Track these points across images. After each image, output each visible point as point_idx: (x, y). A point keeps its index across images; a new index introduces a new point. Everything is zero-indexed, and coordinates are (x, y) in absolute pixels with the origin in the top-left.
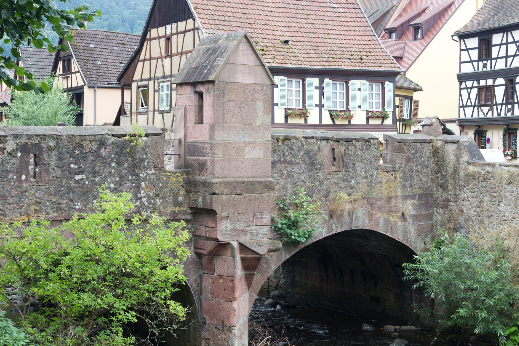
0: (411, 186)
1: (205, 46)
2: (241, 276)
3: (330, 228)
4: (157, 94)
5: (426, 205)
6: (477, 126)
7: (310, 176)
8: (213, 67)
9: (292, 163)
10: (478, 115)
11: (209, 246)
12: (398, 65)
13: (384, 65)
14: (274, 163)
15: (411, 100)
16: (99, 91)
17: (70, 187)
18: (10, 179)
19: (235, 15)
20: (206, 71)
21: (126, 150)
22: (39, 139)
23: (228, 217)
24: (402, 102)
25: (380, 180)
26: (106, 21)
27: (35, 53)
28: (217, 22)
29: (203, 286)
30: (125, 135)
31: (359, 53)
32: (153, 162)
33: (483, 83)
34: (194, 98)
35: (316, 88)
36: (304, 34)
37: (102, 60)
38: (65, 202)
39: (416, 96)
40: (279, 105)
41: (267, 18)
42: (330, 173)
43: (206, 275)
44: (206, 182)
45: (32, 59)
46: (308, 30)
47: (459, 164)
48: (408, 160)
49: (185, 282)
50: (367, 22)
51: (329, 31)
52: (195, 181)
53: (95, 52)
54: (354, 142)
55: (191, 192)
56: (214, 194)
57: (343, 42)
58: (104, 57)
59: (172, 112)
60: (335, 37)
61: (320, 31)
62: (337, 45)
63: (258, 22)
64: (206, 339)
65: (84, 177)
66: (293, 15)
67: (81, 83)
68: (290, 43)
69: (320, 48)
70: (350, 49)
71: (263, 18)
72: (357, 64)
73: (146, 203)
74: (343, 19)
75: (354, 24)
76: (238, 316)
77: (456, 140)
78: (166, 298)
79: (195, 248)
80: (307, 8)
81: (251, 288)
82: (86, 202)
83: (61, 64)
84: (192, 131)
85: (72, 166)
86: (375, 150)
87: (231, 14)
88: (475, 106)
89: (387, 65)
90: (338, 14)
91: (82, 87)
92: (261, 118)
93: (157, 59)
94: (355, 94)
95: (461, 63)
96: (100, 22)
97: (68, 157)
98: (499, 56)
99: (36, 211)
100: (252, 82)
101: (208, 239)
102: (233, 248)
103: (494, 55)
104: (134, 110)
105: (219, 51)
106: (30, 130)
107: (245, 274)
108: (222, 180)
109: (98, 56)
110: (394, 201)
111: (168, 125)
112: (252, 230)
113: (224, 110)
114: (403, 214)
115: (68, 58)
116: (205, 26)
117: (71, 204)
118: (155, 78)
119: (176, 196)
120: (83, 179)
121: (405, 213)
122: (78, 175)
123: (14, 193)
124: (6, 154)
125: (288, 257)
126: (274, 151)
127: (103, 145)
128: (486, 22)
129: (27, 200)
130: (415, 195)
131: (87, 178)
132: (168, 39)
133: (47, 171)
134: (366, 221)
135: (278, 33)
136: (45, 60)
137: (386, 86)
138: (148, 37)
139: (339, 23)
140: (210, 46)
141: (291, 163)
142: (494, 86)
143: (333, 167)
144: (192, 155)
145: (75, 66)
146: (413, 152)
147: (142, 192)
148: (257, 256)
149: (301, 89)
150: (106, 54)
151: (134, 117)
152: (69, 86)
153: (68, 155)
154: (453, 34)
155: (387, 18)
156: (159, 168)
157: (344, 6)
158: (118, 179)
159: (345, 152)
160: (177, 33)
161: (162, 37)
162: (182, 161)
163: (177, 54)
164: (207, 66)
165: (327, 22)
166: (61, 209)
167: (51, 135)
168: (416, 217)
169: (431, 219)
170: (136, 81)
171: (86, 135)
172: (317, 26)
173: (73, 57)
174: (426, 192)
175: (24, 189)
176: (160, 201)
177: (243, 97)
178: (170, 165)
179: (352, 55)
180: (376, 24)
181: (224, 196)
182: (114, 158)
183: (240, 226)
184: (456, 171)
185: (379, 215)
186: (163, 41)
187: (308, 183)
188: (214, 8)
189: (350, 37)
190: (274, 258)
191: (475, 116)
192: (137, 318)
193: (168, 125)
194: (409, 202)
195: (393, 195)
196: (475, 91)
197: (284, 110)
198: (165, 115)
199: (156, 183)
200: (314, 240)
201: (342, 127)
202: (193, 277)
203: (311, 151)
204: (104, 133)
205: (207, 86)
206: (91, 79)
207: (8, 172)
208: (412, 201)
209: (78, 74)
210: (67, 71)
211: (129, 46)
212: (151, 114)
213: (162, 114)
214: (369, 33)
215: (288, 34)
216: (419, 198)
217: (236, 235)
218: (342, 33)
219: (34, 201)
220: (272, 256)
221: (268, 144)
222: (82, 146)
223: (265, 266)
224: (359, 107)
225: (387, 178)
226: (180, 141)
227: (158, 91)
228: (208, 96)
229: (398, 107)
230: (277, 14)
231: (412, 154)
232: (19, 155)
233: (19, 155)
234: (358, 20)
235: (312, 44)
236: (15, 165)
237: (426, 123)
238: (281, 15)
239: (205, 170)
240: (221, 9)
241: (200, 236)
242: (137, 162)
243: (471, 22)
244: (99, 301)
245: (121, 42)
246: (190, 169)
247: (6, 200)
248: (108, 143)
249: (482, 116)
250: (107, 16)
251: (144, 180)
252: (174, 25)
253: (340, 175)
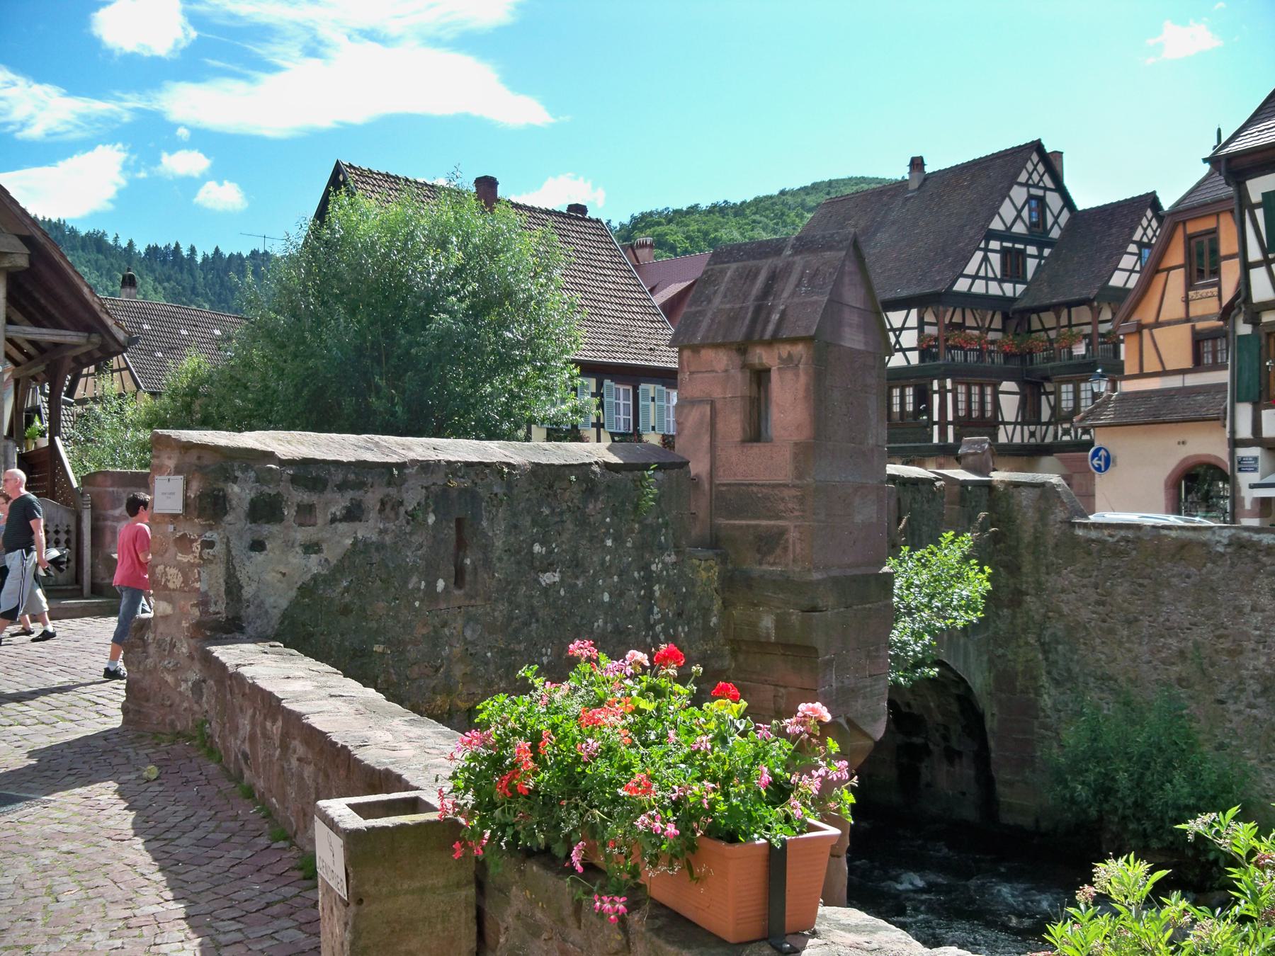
18: (413, 589)
34: (740, 384)
38: (522, 646)
47: (1045, 525)
94: (648, 406)
119: (706, 613)
122: (545, 572)
124: (402, 519)
144: (738, 512)
147: (656, 609)
184: (1038, 539)
233: (431, 519)
239: (778, 551)
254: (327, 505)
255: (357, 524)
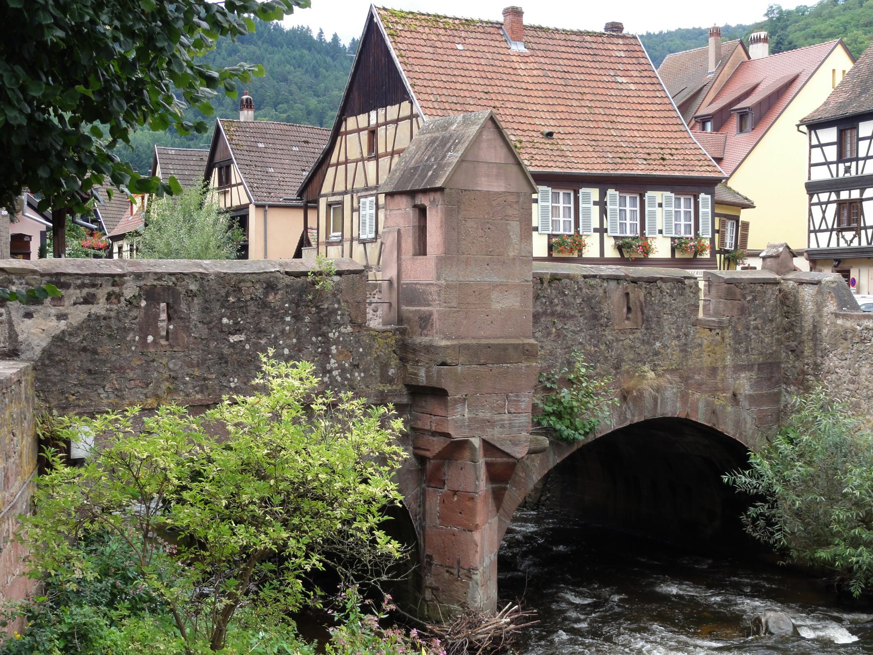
0: (747, 351)
1: (429, 135)
2: (487, 491)
3: (622, 416)
4: (355, 214)
5: (769, 379)
6: (836, 260)
7: (592, 337)
8: (441, 167)
9: (564, 317)
10: (838, 244)
11: (437, 445)
12: (719, 168)
13: (698, 168)
14: (536, 317)
15: (737, 222)
16: (273, 214)
17: (222, 354)
18: (130, 341)
19: (473, 94)
20: (430, 173)
21: (307, 296)
22: (174, 279)
23: (465, 399)
24: (723, 225)
25: (699, 341)
26: (283, 113)
27: (179, 157)
28: (447, 106)
29: (427, 506)
30: (305, 274)
31: (659, 151)
32: (349, 315)
33: (844, 195)
35: (595, 203)
36: (576, 123)
37: (277, 165)
38: (214, 376)
39: (745, 215)
40: (540, 229)
41: (520, 99)
42: (623, 331)
43: (430, 489)
44: (431, 346)
45: (175, 167)
46: (582, 117)
47: (821, 316)
48: (743, 311)
49: (401, 502)
50: (671, 103)
51: (614, 118)
52: (415, 344)
53: (265, 155)
54: (659, 283)
55: (408, 362)
56: (444, 364)
57: (636, 133)
58: (278, 161)
59: (379, 241)
60: (623, 126)
61: (601, 118)
62: (626, 139)
63: (508, 105)
64: (433, 589)
65: (242, 337)
66: (560, 94)
67: (245, 201)
68: (555, 136)
69: (600, 144)
70: (647, 145)
71: (515, 98)
72: (656, 167)
73: (339, 379)
74: (635, 100)
75: (651, 107)
76: (482, 552)
77: (816, 279)
78: (371, 529)
79: (415, 448)
80: (581, 83)
81: (501, 510)
82: (247, 376)
83: (215, 172)
84: (409, 267)
85: (225, 320)
86: (692, 295)
87: (467, 94)
88: (832, 230)
89: (703, 169)
90: (627, 93)
91: (246, 207)
92: (516, 246)
93: (356, 161)
95: (811, 165)
96: (276, 115)
97: (218, 307)
98: (870, 155)
99: (169, 391)
100: (503, 189)
101: (434, 434)
102: (473, 448)
103: (862, 154)
104: (322, 238)
105: (451, 141)
106: (160, 266)
107: (493, 488)
108: (455, 342)
109: (269, 160)
110: (720, 374)
111: (373, 261)
112: (504, 420)
113: (459, 233)
114: (735, 395)
115: (227, 164)
116: (427, 111)
117: (223, 379)
118: (353, 191)
119: (385, 367)
120: (241, 341)
121: (738, 392)
122: (233, 334)
123: (136, 362)
124: (123, 303)
125: (558, 461)
126: (537, 297)
127: (273, 288)
128: (849, 105)
129: (156, 374)
130: (753, 365)
131: (248, 340)
132: (373, 133)
133: (187, 329)
134: (678, 405)
135: (537, 122)
136: (193, 168)
137: (700, 200)
138: (343, 129)
139: (629, 106)
140: (437, 134)
141: (563, 316)
142: (861, 200)
143: (627, 322)
144: (410, 303)
145: (236, 176)
146: (749, 298)
147: (332, 361)
148: (511, 460)
149: (572, 206)
150: (282, 157)
151: (322, 249)
152: (228, 205)
153: (219, 303)
154: (798, 123)
155: (699, 100)
156: (359, 325)
157: (636, 80)
158: (295, 341)
159: (646, 299)
160: (386, 123)
161: (363, 129)
162: (394, 314)
163: (386, 154)
164: (433, 165)
165: (610, 105)
166: (207, 388)
167: (192, 273)
168: (752, 399)
169: (778, 402)
170: (325, 195)
171: (245, 274)
172: (596, 111)
173: (233, 163)
174: (770, 361)
175: (151, 357)
176: (360, 375)
177: (488, 214)
178: (375, 322)
179: (649, 154)
180: (684, 107)
181: (459, 368)
182: (289, 309)
183: (485, 414)
184: (816, 328)
185: (697, 395)
186: (364, 135)
187: (588, 348)
188: (441, 84)
189: (645, 127)
190: (537, 463)
191: (833, 245)
192: (325, 565)
193: (373, 261)
194: (743, 375)
195: (719, 364)
196: (832, 209)
197: (546, 237)
198: (368, 246)
199: (353, 347)
200: (599, 436)
201: (637, 262)
202: (413, 491)
203: (594, 297)
204: (273, 270)
205: (432, 196)
206: (259, 194)
207: (126, 330)
208: (748, 374)
209: (241, 188)
210: (225, 182)
211: (315, 146)
212: (347, 245)
213: (364, 244)
214: (674, 121)
215: (552, 123)
216: (759, 369)
217: (478, 428)
218: (634, 120)
219: (166, 375)
220: (533, 460)
221: (527, 286)
222: (240, 290)
223: (522, 475)
224: (661, 232)
225: (711, 338)
226: (390, 282)
227: (358, 210)
228: (434, 212)
229: (718, 231)
230: (536, 93)
231: (749, 302)
232: (143, 304)
233: (143, 304)
234: (657, 101)
235: (588, 137)
236: (137, 320)
237: (770, 254)
238: (541, 94)
239: (429, 327)
240: (453, 86)
241: (422, 429)
242: (325, 316)
243: (825, 104)
244: (263, 536)
245: (304, 139)
246: (405, 326)
247: (123, 373)
248: (280, 286)
249: (843, 244)
250: (285, 106)
251: (336, 342)
252: (381, 112)
253: (638, 335)
254: (70, 296)
255: (90, 306)
